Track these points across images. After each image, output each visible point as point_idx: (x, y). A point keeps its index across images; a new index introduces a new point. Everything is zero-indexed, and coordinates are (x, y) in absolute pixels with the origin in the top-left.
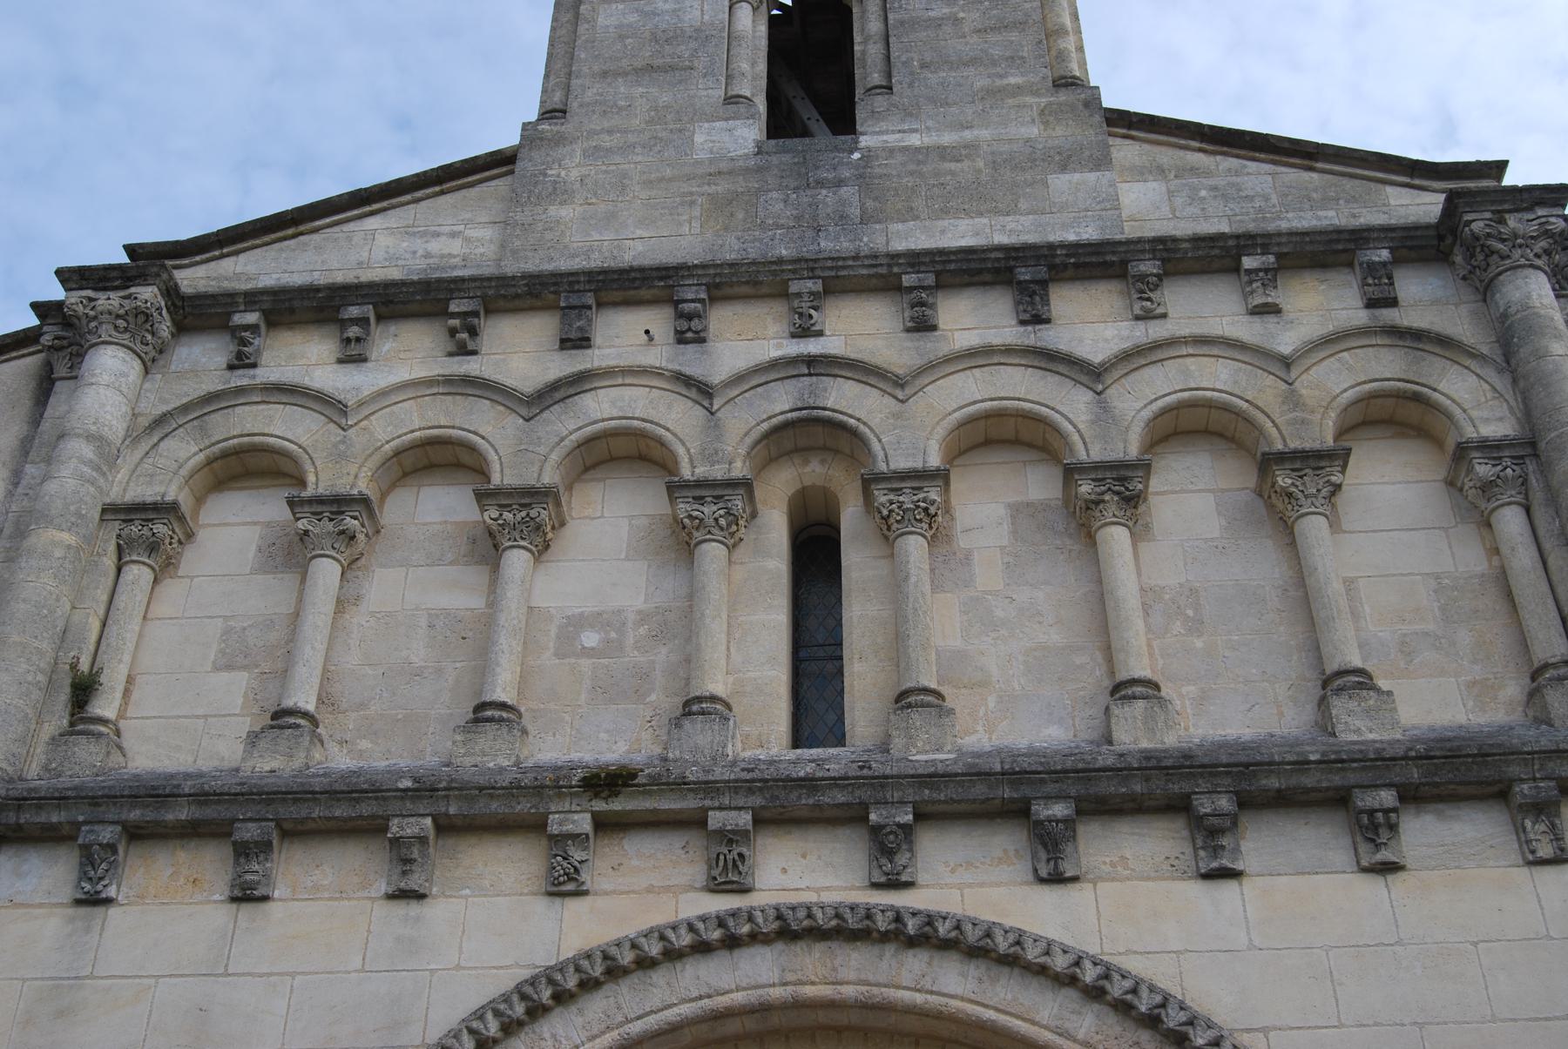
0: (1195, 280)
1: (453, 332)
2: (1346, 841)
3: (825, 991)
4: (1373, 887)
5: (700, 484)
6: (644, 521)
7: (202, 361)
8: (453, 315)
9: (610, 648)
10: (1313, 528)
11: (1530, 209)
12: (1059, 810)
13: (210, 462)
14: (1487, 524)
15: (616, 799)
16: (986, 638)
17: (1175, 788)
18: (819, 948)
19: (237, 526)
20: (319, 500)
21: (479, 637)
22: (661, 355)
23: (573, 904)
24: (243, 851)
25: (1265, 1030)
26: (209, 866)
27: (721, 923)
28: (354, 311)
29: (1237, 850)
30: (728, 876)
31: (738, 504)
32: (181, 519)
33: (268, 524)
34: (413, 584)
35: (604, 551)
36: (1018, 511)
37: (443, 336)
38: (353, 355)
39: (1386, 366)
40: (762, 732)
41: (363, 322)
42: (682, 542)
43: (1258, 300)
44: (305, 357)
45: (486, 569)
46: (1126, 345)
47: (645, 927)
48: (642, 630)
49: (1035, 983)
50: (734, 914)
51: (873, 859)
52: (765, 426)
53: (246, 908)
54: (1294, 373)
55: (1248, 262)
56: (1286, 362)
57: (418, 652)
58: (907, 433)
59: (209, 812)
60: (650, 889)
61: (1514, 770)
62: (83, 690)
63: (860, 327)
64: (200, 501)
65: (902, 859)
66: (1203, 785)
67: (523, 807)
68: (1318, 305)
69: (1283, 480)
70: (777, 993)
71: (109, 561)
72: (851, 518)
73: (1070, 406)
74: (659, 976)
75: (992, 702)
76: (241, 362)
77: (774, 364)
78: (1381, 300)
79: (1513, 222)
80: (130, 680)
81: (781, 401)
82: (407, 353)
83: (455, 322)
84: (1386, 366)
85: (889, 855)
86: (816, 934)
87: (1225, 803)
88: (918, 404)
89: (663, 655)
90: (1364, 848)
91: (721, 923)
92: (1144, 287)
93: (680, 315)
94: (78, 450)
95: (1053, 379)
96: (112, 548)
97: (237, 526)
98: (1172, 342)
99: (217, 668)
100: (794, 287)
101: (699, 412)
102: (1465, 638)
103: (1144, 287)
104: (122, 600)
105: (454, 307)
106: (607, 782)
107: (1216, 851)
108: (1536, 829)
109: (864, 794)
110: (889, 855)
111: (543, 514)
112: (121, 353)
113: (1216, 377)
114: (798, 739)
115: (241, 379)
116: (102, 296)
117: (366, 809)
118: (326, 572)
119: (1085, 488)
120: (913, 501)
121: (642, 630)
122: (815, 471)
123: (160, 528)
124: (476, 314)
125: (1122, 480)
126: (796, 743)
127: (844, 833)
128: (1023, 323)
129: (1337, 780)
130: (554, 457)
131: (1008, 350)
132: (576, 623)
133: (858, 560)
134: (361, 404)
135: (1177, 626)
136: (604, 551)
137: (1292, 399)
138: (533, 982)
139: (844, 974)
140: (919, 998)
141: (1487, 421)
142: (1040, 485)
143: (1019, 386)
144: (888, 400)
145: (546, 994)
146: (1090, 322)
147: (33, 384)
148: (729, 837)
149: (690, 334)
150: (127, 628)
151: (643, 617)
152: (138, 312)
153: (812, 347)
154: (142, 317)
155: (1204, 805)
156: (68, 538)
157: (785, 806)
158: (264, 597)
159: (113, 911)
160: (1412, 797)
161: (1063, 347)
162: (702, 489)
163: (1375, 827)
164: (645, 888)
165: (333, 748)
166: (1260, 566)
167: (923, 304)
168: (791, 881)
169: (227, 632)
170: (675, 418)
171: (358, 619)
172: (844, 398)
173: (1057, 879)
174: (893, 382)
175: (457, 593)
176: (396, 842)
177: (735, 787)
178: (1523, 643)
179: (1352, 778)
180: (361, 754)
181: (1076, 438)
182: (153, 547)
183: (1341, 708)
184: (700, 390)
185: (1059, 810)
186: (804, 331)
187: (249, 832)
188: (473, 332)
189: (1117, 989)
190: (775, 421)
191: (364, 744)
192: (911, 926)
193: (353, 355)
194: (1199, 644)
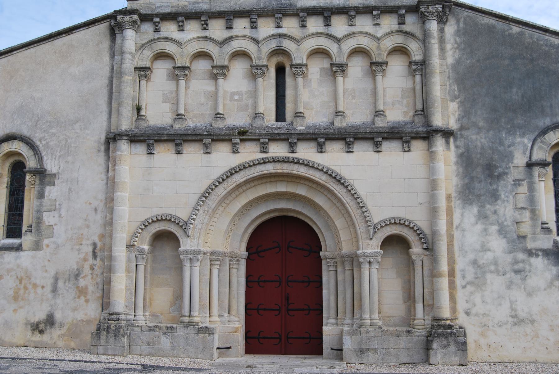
0: (363, 15)
1: (203, 25)
2: (372, 146)
3: (281, 171)
4: (376, 154)
5: (257, 66)
6: (246, 70)
7: (147, 27)
8: (202, 21)
9: (240, 99)
10: (379, 78)
11: (435, 5)
12: (322, 140)
13: (154, 55)
14: (414, 76)
15: (244, 135)
16: (312, 100)
17: (343, 136)
18: (280, 164)
19: (161, 70)
20: (179, 67)
21: (215, 96)
22: (248, 32)
23: (237, 154)
24: (177, 145)
25: (353, 179)
26: (170, 147)
27: (263, 159)
28: (180, 19)
29: (353, 148)
30: (264, 150)
31: (265, 70)
32: (150, 69)
33: (168, 69)
34: (198, 86)
35: (237, 78)
36: (322, 69)
37: (200, 25)
38: (181, 29)
39: (398, 40)
40: (270, 119)
41: (183, 21)
42: (254, 77)
43: (375, 22)
44: (169, 29)
45: (214, 81)
46: (346, 33)
47: (250, 160)
48: (246, 96)
49: (316, 170)
50: (265, 158)
51: (289, 148)
52: (270, 51)
53: (179, 155)
54: (380, 41)
55: (374, 13)
56: (379, 39)
57: (203, 100)
58: (299, 53)
59: (170, 138)
60: (250, 152)
61: (403, 135)
62: (139, 109)
63: (290, 26)
64: (152, 63)
65: (294, 148)
66: (348, 136)
67: (227, 137)
68: (389, 23)
69: (374, 68)
70: (273, 171)
71: (138, 81)
72: (287, 69)
73: (332, 47)
74: (252, 168)
75: (313, 113)
76: (157, 30)
77: (272, 36)
78: (402, 23)
79: (431, 8)
80: (146, 105)
81: (273, 44)
82: (193, 29)
83: (203, 22)
84: (398, 40)
85: (292, 147)
86: (279, 161)
87: (352, 139)
88: (302, 46)
89: (250, 101)
90: (375, 148)
91: (263, 159)
92: (351, 18)
93: (252, 22)
94: (127, 56)
95: (330, 41)
96: (138, 77)
97: (161, 70)
98: (356, 33)
99: (163, 102)
100: (276, 16)
101: (256, 47)
102: (405, 101)
103: (351, 18)
104: (142, 89)
105: (202, 19)
106: (243, 133)
107: (349, 148)
108: (406, 146)
109: (288, 136)
110: (292, 147)
111: (225, 71)
112: (132, 31)
113: (363, 42)
114: (277, 120)
115: (157, 35)
116: (125, 17)
117: (199, 138)
118: (182, 82)
119: (334, 69)
120: (301, 70)
121: (246, 96)
122: (280, 59)
123: (147, 73)
124: (207, 20)
125: (342, 67)
126: (277, 121)
127: (285, 142)
128: (325, 26)
129: (372, 136)
130: (227, 57)
131: (321, 34)
132: (233, 94)
133: (289, 80)
134: (185, 43)
135: (350, 98)
136: (237, 78)
137: (379, 48)
138: (231, 169)
139: (284, 168)
140: (296, 173)
141: (417, 55)
142: (326, 64)
143: (323, 43)
144: (296, 45)
145: (234, 172)
146: (339, 27)
147: (109, 31)
148: (264, 144)
149: (254, 26)
150: (144, 95)
151: (247, 92)
152: (134, 21)
153: (280, 31)
154: (134, 23)
155: (348, 140)
156: (130, 78)
157: (275, 138)
158: (170, 86)
159: (155, 155)
160: (384, 138)
161: (333, 33)
162: (258, 67)
163: (377, 144)
164: (249, 152)
165: (188, 120)
166: (367, 85)
167: (304, 21)
168: (275, 151)
169: (163, 94)
170: (251, 48)
171: (190, 91)
172: (287, 44)
173: (321, 152)
174: (297, 41)
175: (208, 86)
176: (204, 144)
177: (265, 135)
178: (415, 105)
179: (374, 136)
180: (194, 122)
181: (333, 56)
182: (146, 77)
183: (377, 119)
184: (256, 41)
185: (322, 140)
186: (278, 27)
187: (178, 141)
188: (207, 25)
189: (329, 172)
190: (272, 50)
191: (194, 119)
192: (296, 161)
193: (181, 29)
194: (354, 101)
